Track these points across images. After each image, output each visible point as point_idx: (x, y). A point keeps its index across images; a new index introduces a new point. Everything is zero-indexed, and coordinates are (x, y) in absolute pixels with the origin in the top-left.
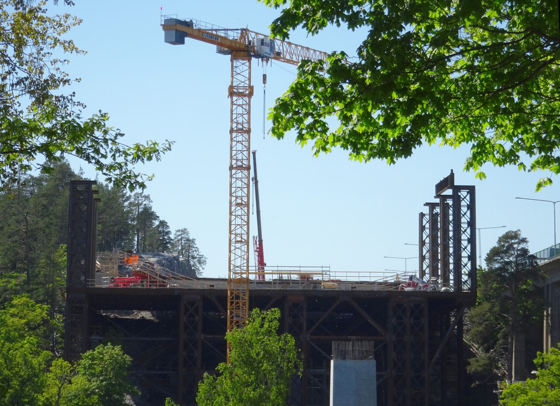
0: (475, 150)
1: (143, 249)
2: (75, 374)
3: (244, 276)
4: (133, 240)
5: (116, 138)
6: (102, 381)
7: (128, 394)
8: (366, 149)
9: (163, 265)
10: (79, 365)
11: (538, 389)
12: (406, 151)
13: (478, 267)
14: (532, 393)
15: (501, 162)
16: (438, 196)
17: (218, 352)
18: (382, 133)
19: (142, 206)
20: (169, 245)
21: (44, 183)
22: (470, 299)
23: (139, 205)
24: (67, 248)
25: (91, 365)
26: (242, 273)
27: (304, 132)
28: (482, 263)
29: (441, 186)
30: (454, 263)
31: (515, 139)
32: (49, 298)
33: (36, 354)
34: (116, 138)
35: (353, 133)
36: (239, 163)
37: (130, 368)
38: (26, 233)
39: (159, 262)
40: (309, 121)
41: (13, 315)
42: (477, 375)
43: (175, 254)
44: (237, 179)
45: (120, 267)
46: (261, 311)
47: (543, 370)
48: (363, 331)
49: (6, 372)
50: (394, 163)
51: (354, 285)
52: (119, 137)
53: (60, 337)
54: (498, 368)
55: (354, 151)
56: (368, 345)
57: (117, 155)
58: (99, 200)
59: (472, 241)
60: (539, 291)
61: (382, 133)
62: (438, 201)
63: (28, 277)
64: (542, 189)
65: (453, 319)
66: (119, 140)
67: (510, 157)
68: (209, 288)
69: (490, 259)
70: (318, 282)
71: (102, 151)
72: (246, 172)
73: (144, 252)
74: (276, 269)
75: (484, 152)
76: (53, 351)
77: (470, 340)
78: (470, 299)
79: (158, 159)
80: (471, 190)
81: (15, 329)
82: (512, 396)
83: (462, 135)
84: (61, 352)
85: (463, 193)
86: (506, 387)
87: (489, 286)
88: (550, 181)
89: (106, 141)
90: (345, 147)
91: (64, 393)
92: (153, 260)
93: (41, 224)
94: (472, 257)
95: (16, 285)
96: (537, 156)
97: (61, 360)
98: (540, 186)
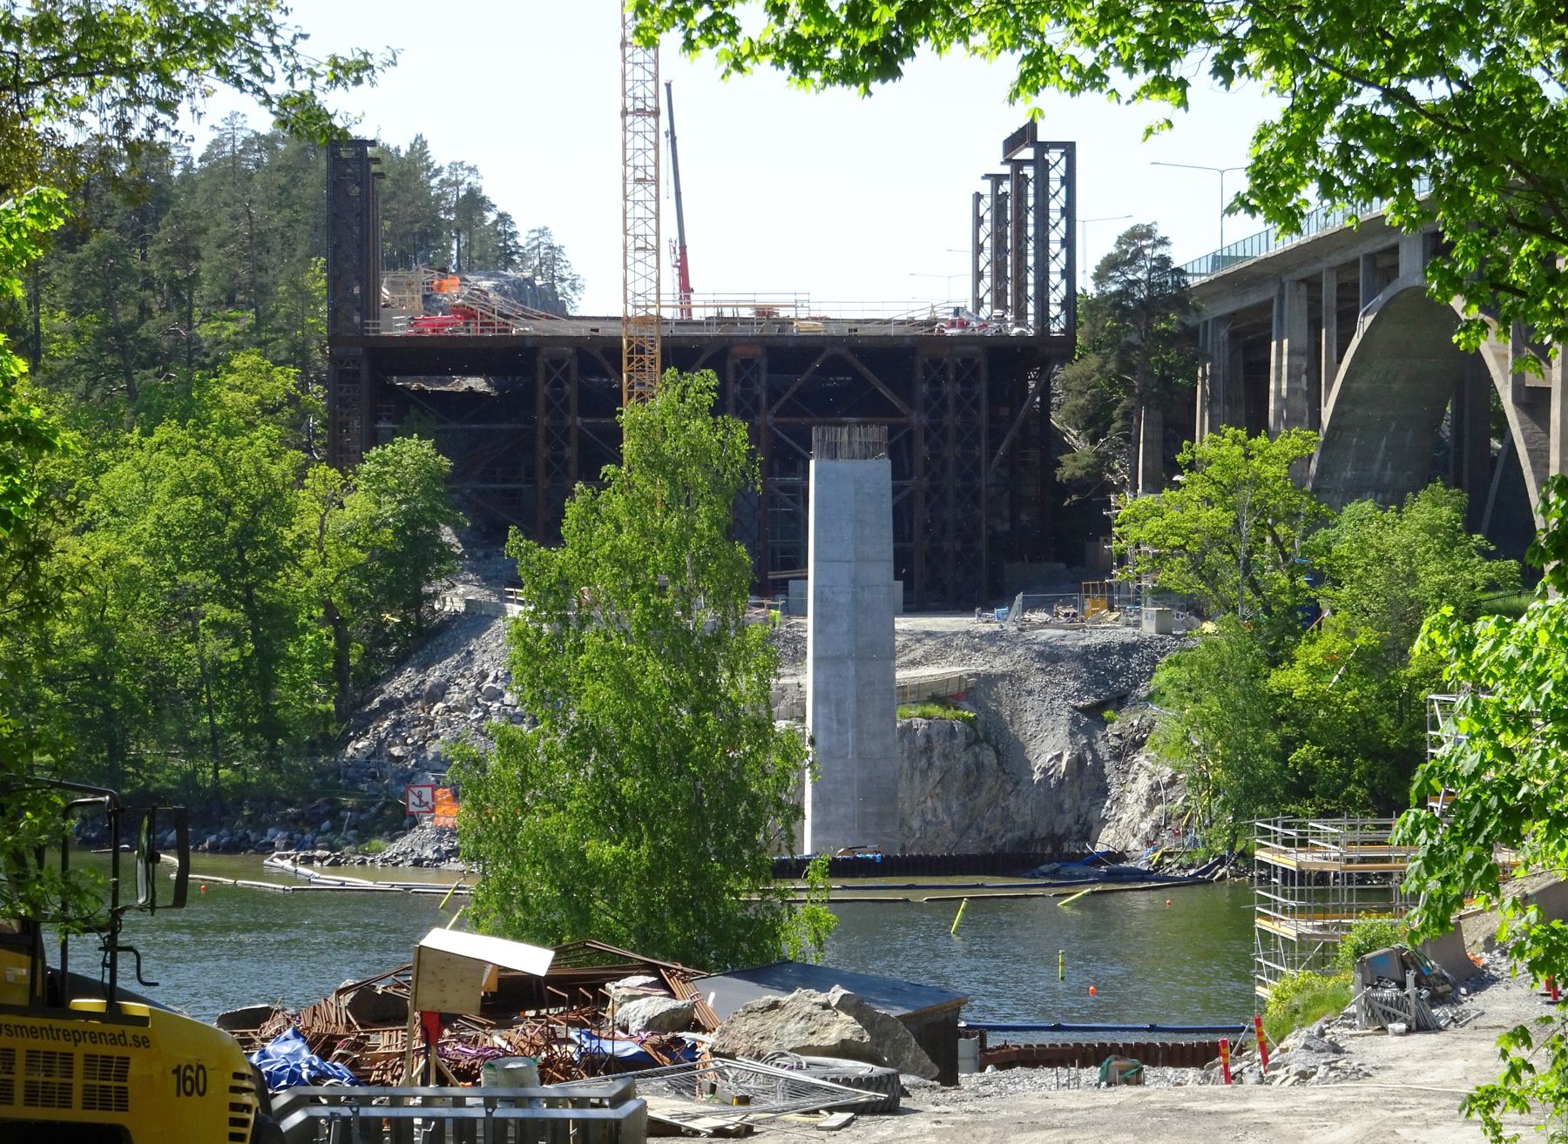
0: (1024, 66)
1: (469, 264)
2: (349, 492)
3: (653, 311)
4: (450, 248)
5: (294, 42)
6: (400, 502)
7: (447, 524)
8: (819, 68)
9: (505, 294)
10: (356, 474)
11: (1182, 507)
12: (888, 70)
13: (1079, 291)
14: (1172, 515)
15: (1075, 89)
16: (1007, 161)
17: (606, 444)
18: (847, 39)
19: (465, 186)
20: (515, 257)
21: (281, 146)
22: (1064, 349)
23: (457, 184)
24: (326, 263)
25: (379, 474)
26: (647, 307)
27: (695, 35)
28: (1086, 284)
29: (1013, 143)
30: (1036, 284)
31: (1102, 46)
32: (299, 356)
33: (274, 456)
34: (294, 42)
35: (793, 38)
36: (640, 105)
37: (448, 480)
38: (251, 238)
39: (496, 289)
40: (704, 13)
41: (232, 388)
42: (1073, 485)
43: (527, 274)
44: (635, 133)
45: (426, 298)
46: (680, 373)
47: (1194, 475)
48: (866, 406)
49: (224, 491)
50: (870, 94)
51: (595, 325)
52: (299, 40)
53: (321, 425)
54: (1113, 472)
55: (794, 72)
56: (876, 433)
57: (297, 76)
58: (381, 175)
59: (1069, 243)
60: (1190, 335)
61: (847, 39)
62: (1007, 170)
63: (257, 319)
64: (1151, 137)
65: (1032, 385)
66: (301, 46)
67: (1093, 77)
68: (590, 333)
69: (1100, 277)
70: (788, 322)
71: (266, 70)
72: (651, 120)
73: (470, 270)
74: (711, 298)
75: (1040, 69)
76: (308, 450)
77: (1062, 423)
78: (1064, 349)
79: (373, 84)
80: (1069, 149)
81: (238, 413)
82: (1137, 520)
83: (1001, 38)
84: (324, 452)
85: (1053, 156)
86: (1126, 505)
87: (1100, 325)
88: (1170, 124)
89: (275, 50)
90: (778, 64)
91: (330, 524)
92: (486, 284)
93: (276, 222)
94: (1069, 273)
95: (236, 334)
96: (1144, 77)
97: (324, 467)
98: (1149, 131)
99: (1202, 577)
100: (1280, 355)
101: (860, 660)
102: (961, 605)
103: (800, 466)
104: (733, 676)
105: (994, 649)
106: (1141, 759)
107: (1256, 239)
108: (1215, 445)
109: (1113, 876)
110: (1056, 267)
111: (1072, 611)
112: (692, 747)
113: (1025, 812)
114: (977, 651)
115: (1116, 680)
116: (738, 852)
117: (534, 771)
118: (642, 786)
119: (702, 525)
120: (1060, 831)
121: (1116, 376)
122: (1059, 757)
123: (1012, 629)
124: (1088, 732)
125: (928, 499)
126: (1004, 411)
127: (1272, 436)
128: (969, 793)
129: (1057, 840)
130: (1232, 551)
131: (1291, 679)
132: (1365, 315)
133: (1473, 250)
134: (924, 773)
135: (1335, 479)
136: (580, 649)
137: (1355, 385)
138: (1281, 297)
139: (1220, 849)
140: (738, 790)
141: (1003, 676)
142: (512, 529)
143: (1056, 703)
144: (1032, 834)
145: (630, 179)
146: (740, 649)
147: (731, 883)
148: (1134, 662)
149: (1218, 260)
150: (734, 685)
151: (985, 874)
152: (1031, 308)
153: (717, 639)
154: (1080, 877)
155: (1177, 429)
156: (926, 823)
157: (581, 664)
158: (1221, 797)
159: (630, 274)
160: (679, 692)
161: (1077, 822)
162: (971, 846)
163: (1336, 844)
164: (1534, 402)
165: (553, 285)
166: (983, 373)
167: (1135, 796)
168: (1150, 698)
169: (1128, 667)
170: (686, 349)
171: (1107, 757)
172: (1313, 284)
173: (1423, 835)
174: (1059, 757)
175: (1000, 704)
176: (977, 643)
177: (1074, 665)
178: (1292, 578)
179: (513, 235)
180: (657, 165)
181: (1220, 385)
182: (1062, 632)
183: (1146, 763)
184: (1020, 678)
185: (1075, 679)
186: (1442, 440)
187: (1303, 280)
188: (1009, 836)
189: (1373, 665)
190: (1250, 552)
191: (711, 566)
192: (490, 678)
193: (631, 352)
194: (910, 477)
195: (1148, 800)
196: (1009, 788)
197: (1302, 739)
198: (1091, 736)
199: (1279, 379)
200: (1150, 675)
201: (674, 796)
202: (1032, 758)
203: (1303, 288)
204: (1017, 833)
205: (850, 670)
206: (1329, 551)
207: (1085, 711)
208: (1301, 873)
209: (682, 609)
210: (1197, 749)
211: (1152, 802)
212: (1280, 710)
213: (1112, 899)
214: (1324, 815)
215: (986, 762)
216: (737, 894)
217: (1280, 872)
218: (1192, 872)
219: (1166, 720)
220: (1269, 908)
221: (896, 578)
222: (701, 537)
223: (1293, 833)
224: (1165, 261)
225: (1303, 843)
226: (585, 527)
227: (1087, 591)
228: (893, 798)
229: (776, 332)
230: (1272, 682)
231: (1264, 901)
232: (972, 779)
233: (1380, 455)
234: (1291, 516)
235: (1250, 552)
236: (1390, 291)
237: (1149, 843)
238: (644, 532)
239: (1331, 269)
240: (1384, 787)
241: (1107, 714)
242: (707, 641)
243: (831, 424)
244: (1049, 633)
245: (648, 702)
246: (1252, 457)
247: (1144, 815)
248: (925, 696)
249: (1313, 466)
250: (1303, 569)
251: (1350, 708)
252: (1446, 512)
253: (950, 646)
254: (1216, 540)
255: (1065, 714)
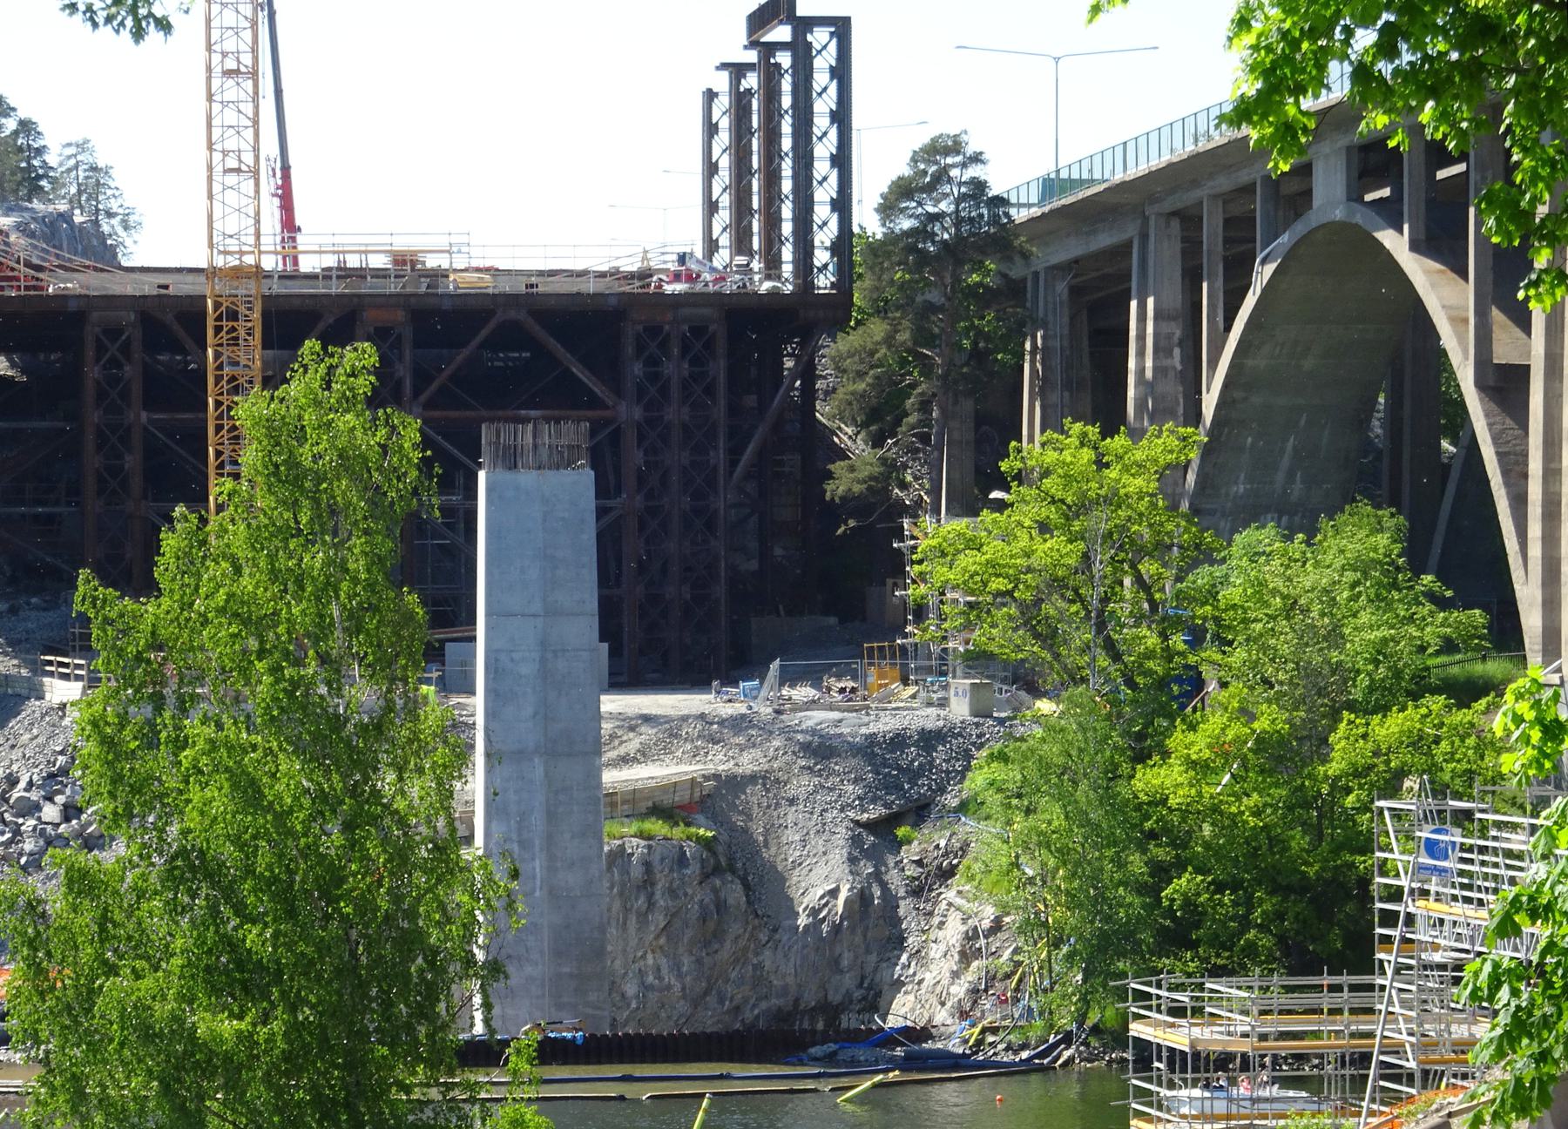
3: (249, 260)
9: (32, 235)
13: (856, 230)
14: (994, 548)
20: (44, 183)
22: (834, 313)
30: (795, 220)
43: (62, 207)
46: (324, 348)
48: (560, 397)
54: (904, 486)
56: (573, 432)
59: (842, 160)
60: (1013, 290)
62: (752, 56)
64: (1101, 16)
65: (789, 363)
69: (888, 208)
70: (439, 275)
77: (832, 418)
78: (834, 313)
80: (841, 28)
86: (931, 532)
94: (842, 205)
99: (1037, 636)
100: (1143, 321)
101: (554, 752)
102: (692, 677)
103: (460, 480)
104: (401, 779)
105: (741, 740)
106: (950, 895)
107: (1108, 155)
108: (1050, 449)
109: (909, 1063)
110: (823, 195)
111: (851, 684)
112: (343, 880)
113: (785, 971)
114: (716, 743)
115: (913, 783)
116: (410, 1029)
117: (118, 916)
118: (276, 935)
119: (358, 565)
120: (835, 998)
121: (909, 351)
122: (834, 893)
123: (766, 711)
124: (874, 855)
125: (642, 526)
126: (751, 400)
127: (1136, 435)
128: (707, 944)
129: (831, 1011)
130: (1079, 598)
131: (1163, 779)
132: (1263, 262)
133: (1545, 172)
134: (643, 917)
135: (1219, 499)
136: (180, 744)
137: (1250, 362)
138: (1144, 237)
139: (1065, 1022)
140: (411, 941)
141: (753, 778)
142: (84, 573)
143: (829, 816)
144: (797, 1001)
145: (217, 70)
146: (410, 741)
147: (400, 1072)
148: (940, 755)
149: (1051, 186)
150: (403, 793)
151: (731, 1060)
152: (787, 253)
153: (377, 728)
154: (867, 1062)
155: (1001, 427)
156: (648, 988)
157: (185, 763)
158: (1065, 949)
159: (217, 206)
160: (324, 802)
161: (860, 985)
162: (710, 1021)
163: (1245, 1013)
164: (1506, 386)
165: (96, 223)
166: (721, 346)
167: (942, 947)
168: (963, 807)
169: (931, 763)
170: (300, 317)
171: (902, 893)
172: (1189, 220)
173: (1504, 994)
174: (834, 893)
175: (750, 818)
176: (714, 731)
177: (853, 762)
178: (1164, 636)
179: (40, 151)
180: (254, 50)
181: (1056, 361)
182: (836, 715)
183: (959, 901)
184: (777, 781)
185: (855, 781)
186: (1370, 442)
187: (1174, 214)
188: (764, 1005)
189: (1279, 759)
190: (1105, 600)
191: (371, 623)
192: (22, 784)
193: (219, 318)
194: (619, 491)
195: (962, 953)
196: (763, 937)
197: (1180, 866)
198: (879, 863)
199: (1141, 353)
200: (962, 774)
201: (319, 950)
202: (795, 894)
203: (1175, 224)
204: (775, 1002)
205: (538, 769)
206: (1215, 596)
207: (870, 826)
208: (1196, 1055)
209: (329, 684)
210: (1031, 881)
211: (966, 957)
212: (1148, 825)
213: (908, 1097)
214: (1217, 972)
215: (731, 901)
216: (407, 1090)
217: (1165, 1054)
218: (1025, 1055)
219: (985, 839)
220: (1150, 1105)
221: (602, 640)
222: (355, 581)
223: (1183, 998)
224: (979, 186)
225: (1198, 1011)
226: (190, 564)
227: (871, 657)
228: (600, 953)
229: (423, 289)
230: (1138, 784)
231: (1142, 1094)
232: (711, 925)
233: (1286, 462)
234: (1160, 549)
235: (1105, 600)
236: (1299, 228)
237: (963, 1015)
238: (274, 575)
239: (1215, 197)
240: (1298, 933)
241: (901, 832)
242: (363, 729)
243: (507, 420)
244: (816, 717)
245: (282, 817)
246: (1107, 465)
247: (956, 975)
248: (644, 806)
249: (1191, 478)
250: (1176, 623)
251: (1252, 821)
252: (1382, 540)
253: (676, 736)
254: (1057, 584)
255: (842, 833)
